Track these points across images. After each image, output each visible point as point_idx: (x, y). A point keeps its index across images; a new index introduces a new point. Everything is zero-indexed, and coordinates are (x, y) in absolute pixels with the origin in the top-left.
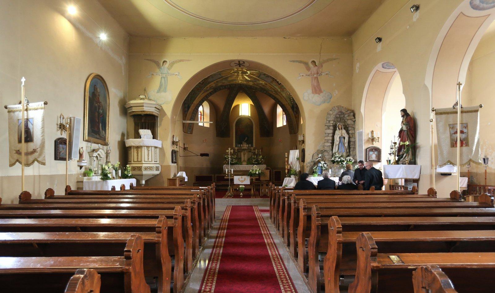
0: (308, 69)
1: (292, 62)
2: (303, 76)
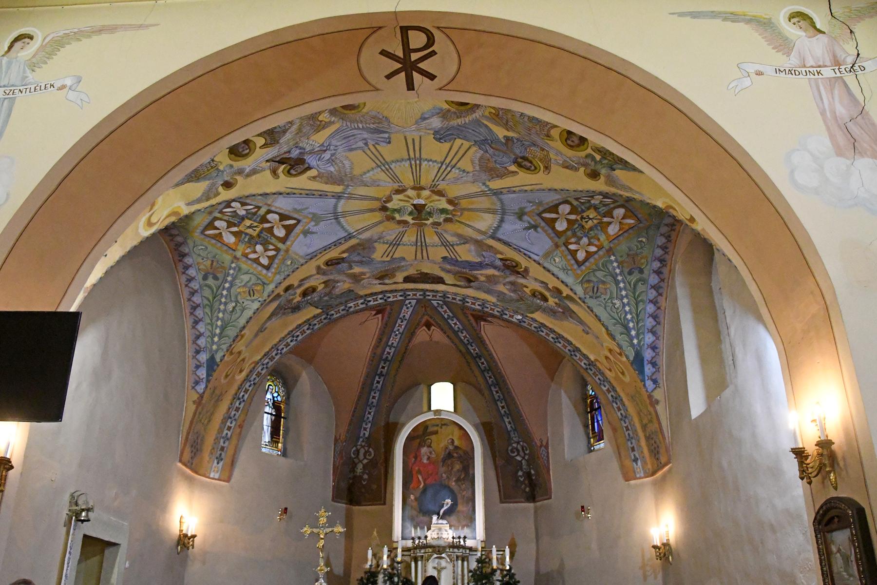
0: (784, 45)
1: (688, 19)
2: (759, 73)
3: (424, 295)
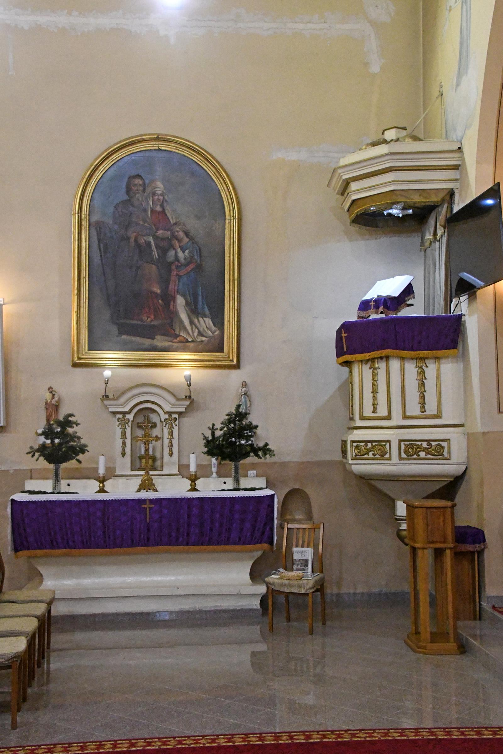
3: (158, 439)
